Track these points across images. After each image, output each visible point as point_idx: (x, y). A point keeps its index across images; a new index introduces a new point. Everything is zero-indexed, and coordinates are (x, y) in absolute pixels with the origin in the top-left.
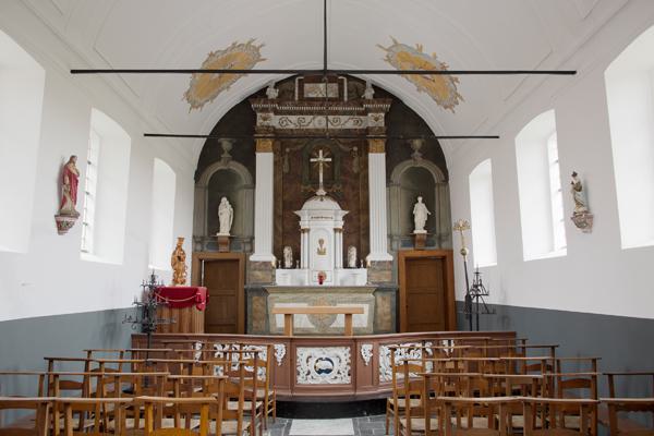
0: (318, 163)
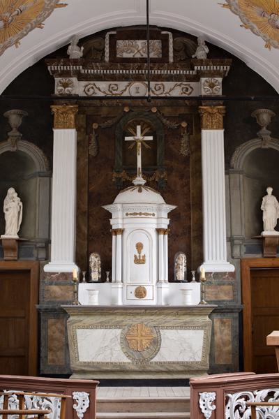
0: (135, 142)
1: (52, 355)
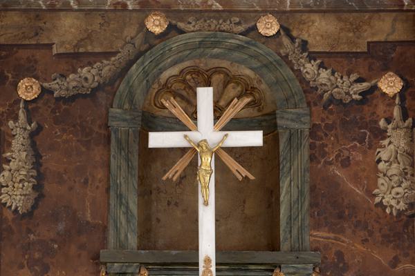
0: (190, 154)
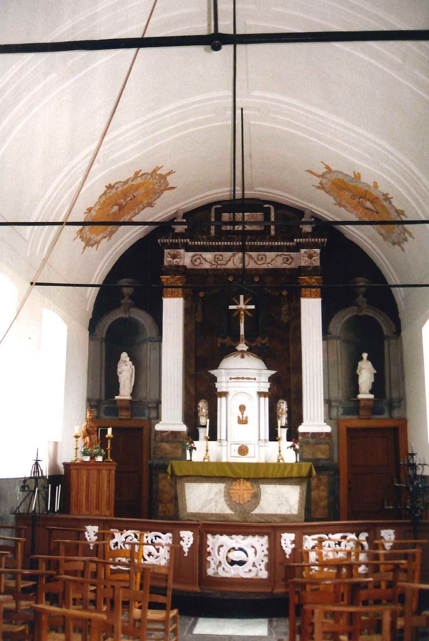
0: (239, 310)
1: (163, 507)
